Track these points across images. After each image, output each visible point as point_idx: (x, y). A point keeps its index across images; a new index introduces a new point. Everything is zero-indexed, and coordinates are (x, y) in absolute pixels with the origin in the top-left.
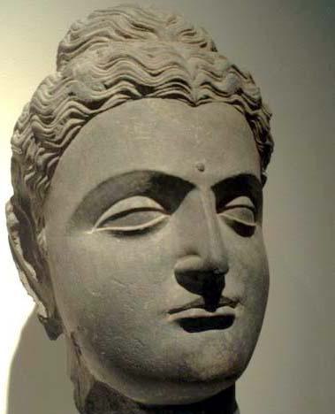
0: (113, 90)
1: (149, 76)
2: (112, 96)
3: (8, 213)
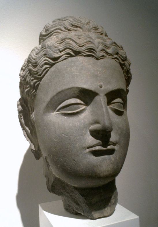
0: (63, 53)
2: (62, 55)
3: (18, 106)
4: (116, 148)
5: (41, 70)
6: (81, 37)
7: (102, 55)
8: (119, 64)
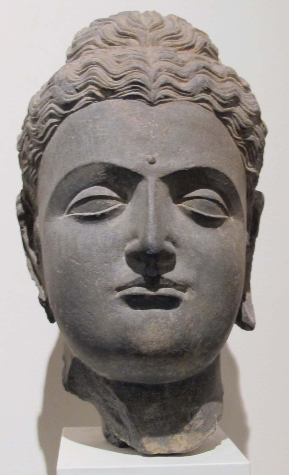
0: (82, 93)
1: (111, 80)
2: (82, 98)
3: (17, 204)
4: (185, 296)
5: (43, 128)
6: (123, 59)
7: (163, 95)
8: (213, 115)
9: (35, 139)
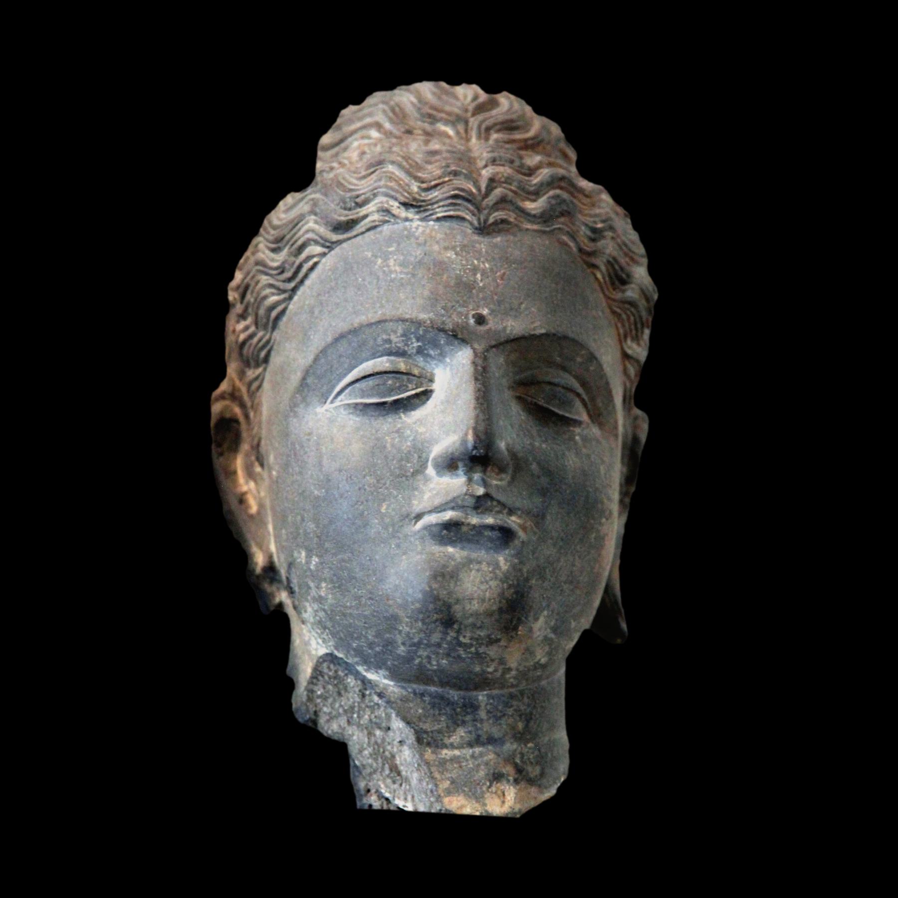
9: (278, 280)
